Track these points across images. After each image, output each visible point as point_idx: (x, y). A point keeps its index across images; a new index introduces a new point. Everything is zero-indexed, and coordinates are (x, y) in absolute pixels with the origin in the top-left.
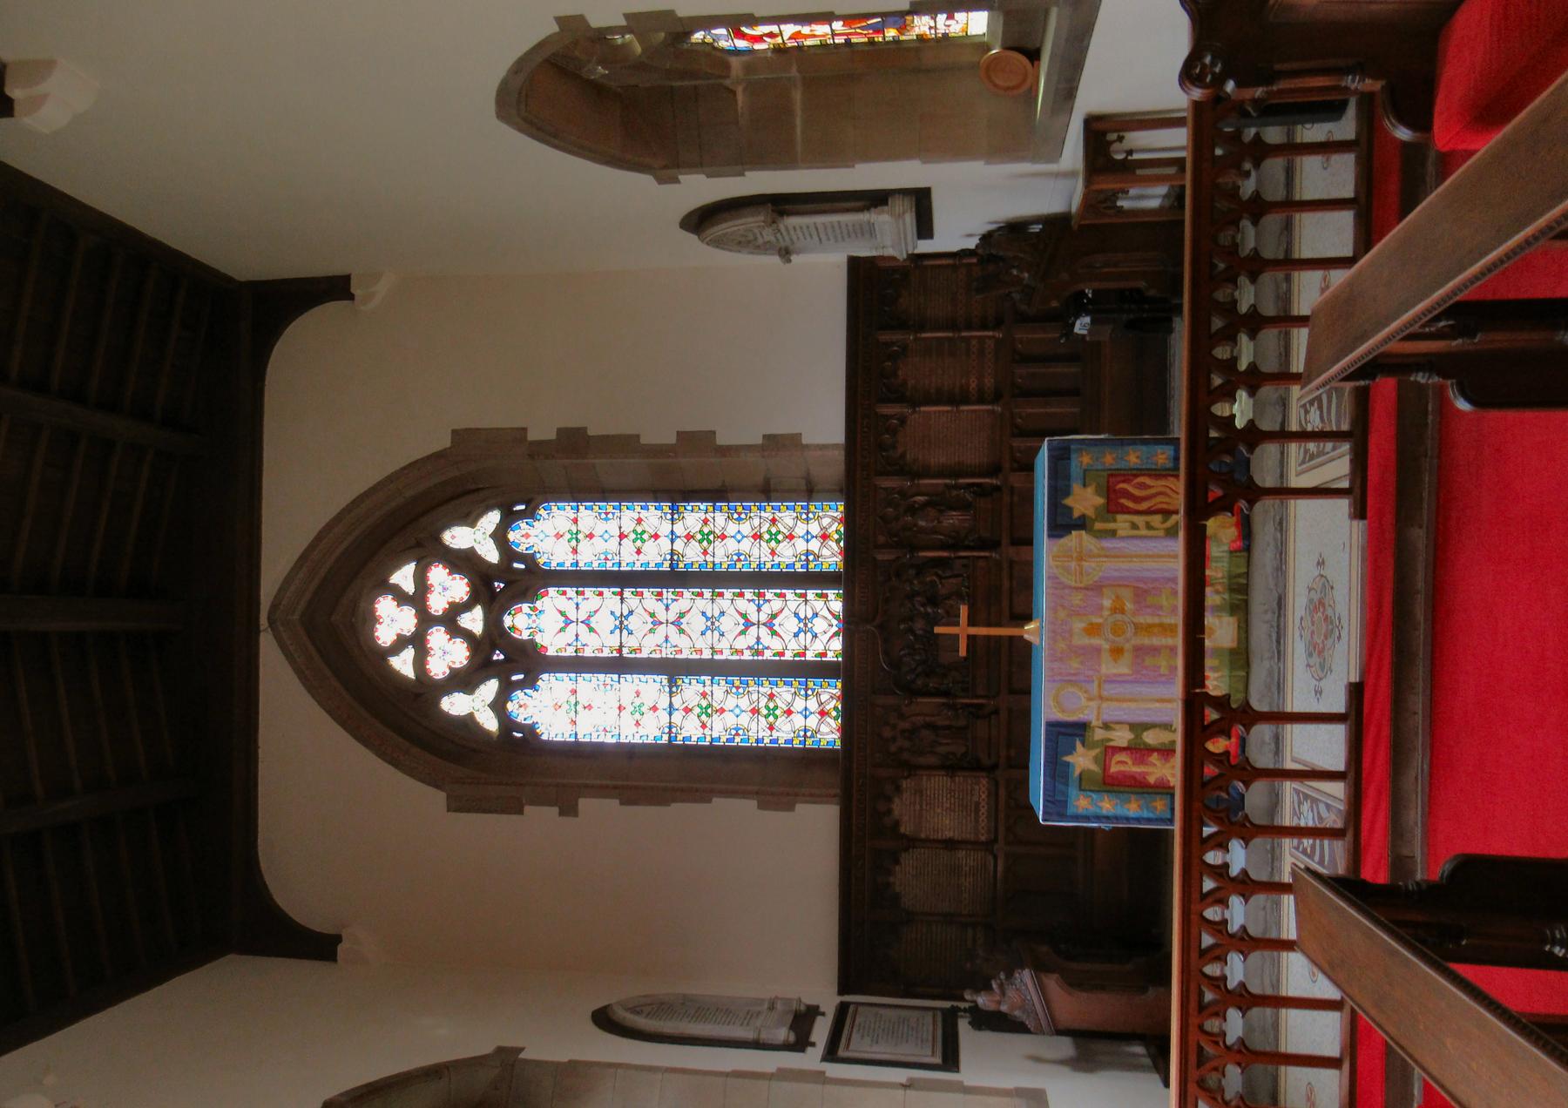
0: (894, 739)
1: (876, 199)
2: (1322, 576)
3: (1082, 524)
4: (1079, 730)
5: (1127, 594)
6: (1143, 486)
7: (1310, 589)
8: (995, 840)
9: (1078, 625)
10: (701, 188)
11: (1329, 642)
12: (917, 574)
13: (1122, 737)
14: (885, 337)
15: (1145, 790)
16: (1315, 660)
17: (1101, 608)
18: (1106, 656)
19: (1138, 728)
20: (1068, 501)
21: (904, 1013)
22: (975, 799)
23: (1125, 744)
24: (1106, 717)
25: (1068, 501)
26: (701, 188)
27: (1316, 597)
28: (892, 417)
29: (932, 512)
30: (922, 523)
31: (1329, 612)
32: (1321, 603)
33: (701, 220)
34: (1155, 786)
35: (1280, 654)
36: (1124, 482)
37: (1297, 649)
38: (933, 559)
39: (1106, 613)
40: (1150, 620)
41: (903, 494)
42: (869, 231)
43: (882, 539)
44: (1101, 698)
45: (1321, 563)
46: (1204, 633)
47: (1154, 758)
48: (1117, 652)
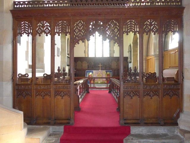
1: (131, 59)
3: (106, 73)
33: (130, 45)
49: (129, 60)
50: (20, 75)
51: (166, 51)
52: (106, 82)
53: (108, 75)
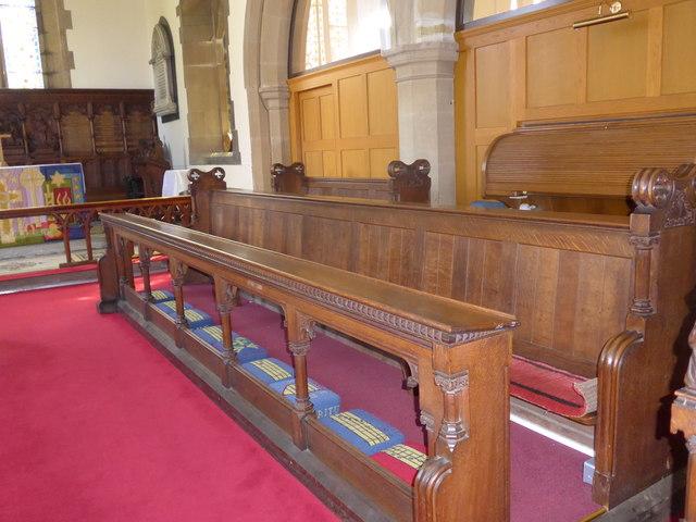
1: (175, 99)
3: (48, 179)
10: (175, 25)
20: (57, 173)
25: (57, 173)
26: (175, 25)
33: (164, 25)
42: (163, 97)
43: (28, 106)
49: (161, 104)
50: (218, 174)
51: (296, 75)
52: (53, 231)
53: (58, 191)
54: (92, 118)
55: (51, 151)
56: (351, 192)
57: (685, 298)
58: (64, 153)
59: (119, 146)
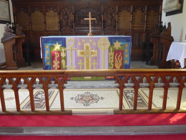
0: (65, 10)
2: (99, 99)
3: (112, 45)
4: (64, 45)
5: (96, 55)
6: (120, 58)
7: (96, 95)
8: (47, 31)
9: (88, 44)
11: (83, 102)
12: (98, 14)
13: (63, 55)
14: (146, 7)
15: (51, 60)
16: (80, 97)
17: (92, 50)
18: (82, 51)
19: (65, 58)
20: (117, 41)
21: (8, 13)
22: (55, 27)
23: (61, 56)
24: (67, 51)
25: (117, 41)
27: (94, 97)
28: (130, 9)
29: (111, 17)
30: (109, 15)
31: (91, 101)
32: (93, 99)
34: (52, 62)
35: (82, 88)
36: (121, 53)
37: (82, 92)
38: (101, 18)
39: (91, 51)
40: (90, 60)
41: (115, 11)
43: (105, 7)
44: (72, 50)
45: (102, 98)
46: (94, 34)
47: (59, 62)
48: (82, 53)
54: (132, 13)
55: (112, 28)
56: (70, 73)
57: (171, 40)
58: (118, 30)
59: (141, 27)
